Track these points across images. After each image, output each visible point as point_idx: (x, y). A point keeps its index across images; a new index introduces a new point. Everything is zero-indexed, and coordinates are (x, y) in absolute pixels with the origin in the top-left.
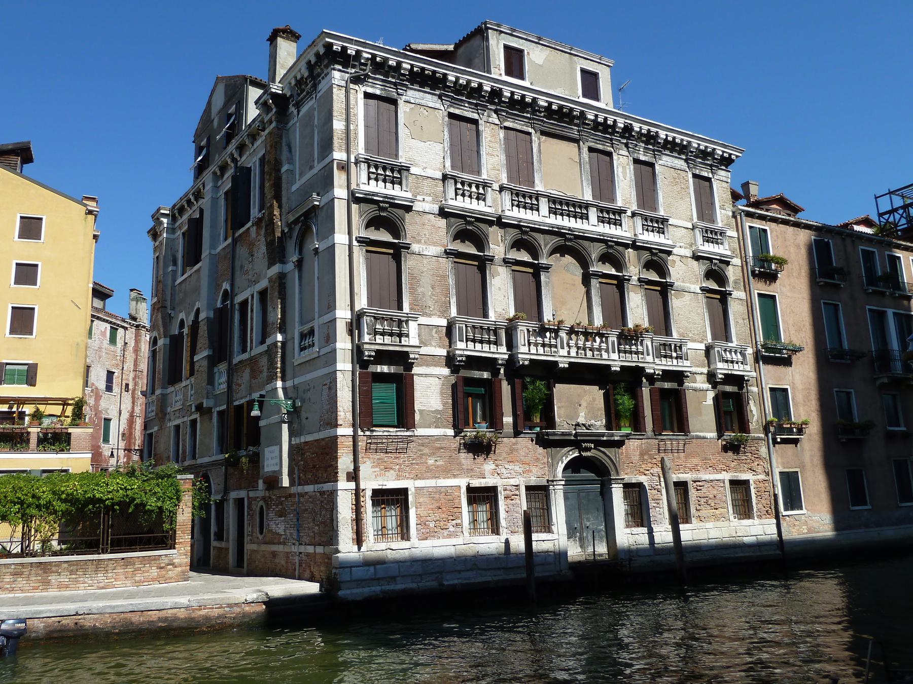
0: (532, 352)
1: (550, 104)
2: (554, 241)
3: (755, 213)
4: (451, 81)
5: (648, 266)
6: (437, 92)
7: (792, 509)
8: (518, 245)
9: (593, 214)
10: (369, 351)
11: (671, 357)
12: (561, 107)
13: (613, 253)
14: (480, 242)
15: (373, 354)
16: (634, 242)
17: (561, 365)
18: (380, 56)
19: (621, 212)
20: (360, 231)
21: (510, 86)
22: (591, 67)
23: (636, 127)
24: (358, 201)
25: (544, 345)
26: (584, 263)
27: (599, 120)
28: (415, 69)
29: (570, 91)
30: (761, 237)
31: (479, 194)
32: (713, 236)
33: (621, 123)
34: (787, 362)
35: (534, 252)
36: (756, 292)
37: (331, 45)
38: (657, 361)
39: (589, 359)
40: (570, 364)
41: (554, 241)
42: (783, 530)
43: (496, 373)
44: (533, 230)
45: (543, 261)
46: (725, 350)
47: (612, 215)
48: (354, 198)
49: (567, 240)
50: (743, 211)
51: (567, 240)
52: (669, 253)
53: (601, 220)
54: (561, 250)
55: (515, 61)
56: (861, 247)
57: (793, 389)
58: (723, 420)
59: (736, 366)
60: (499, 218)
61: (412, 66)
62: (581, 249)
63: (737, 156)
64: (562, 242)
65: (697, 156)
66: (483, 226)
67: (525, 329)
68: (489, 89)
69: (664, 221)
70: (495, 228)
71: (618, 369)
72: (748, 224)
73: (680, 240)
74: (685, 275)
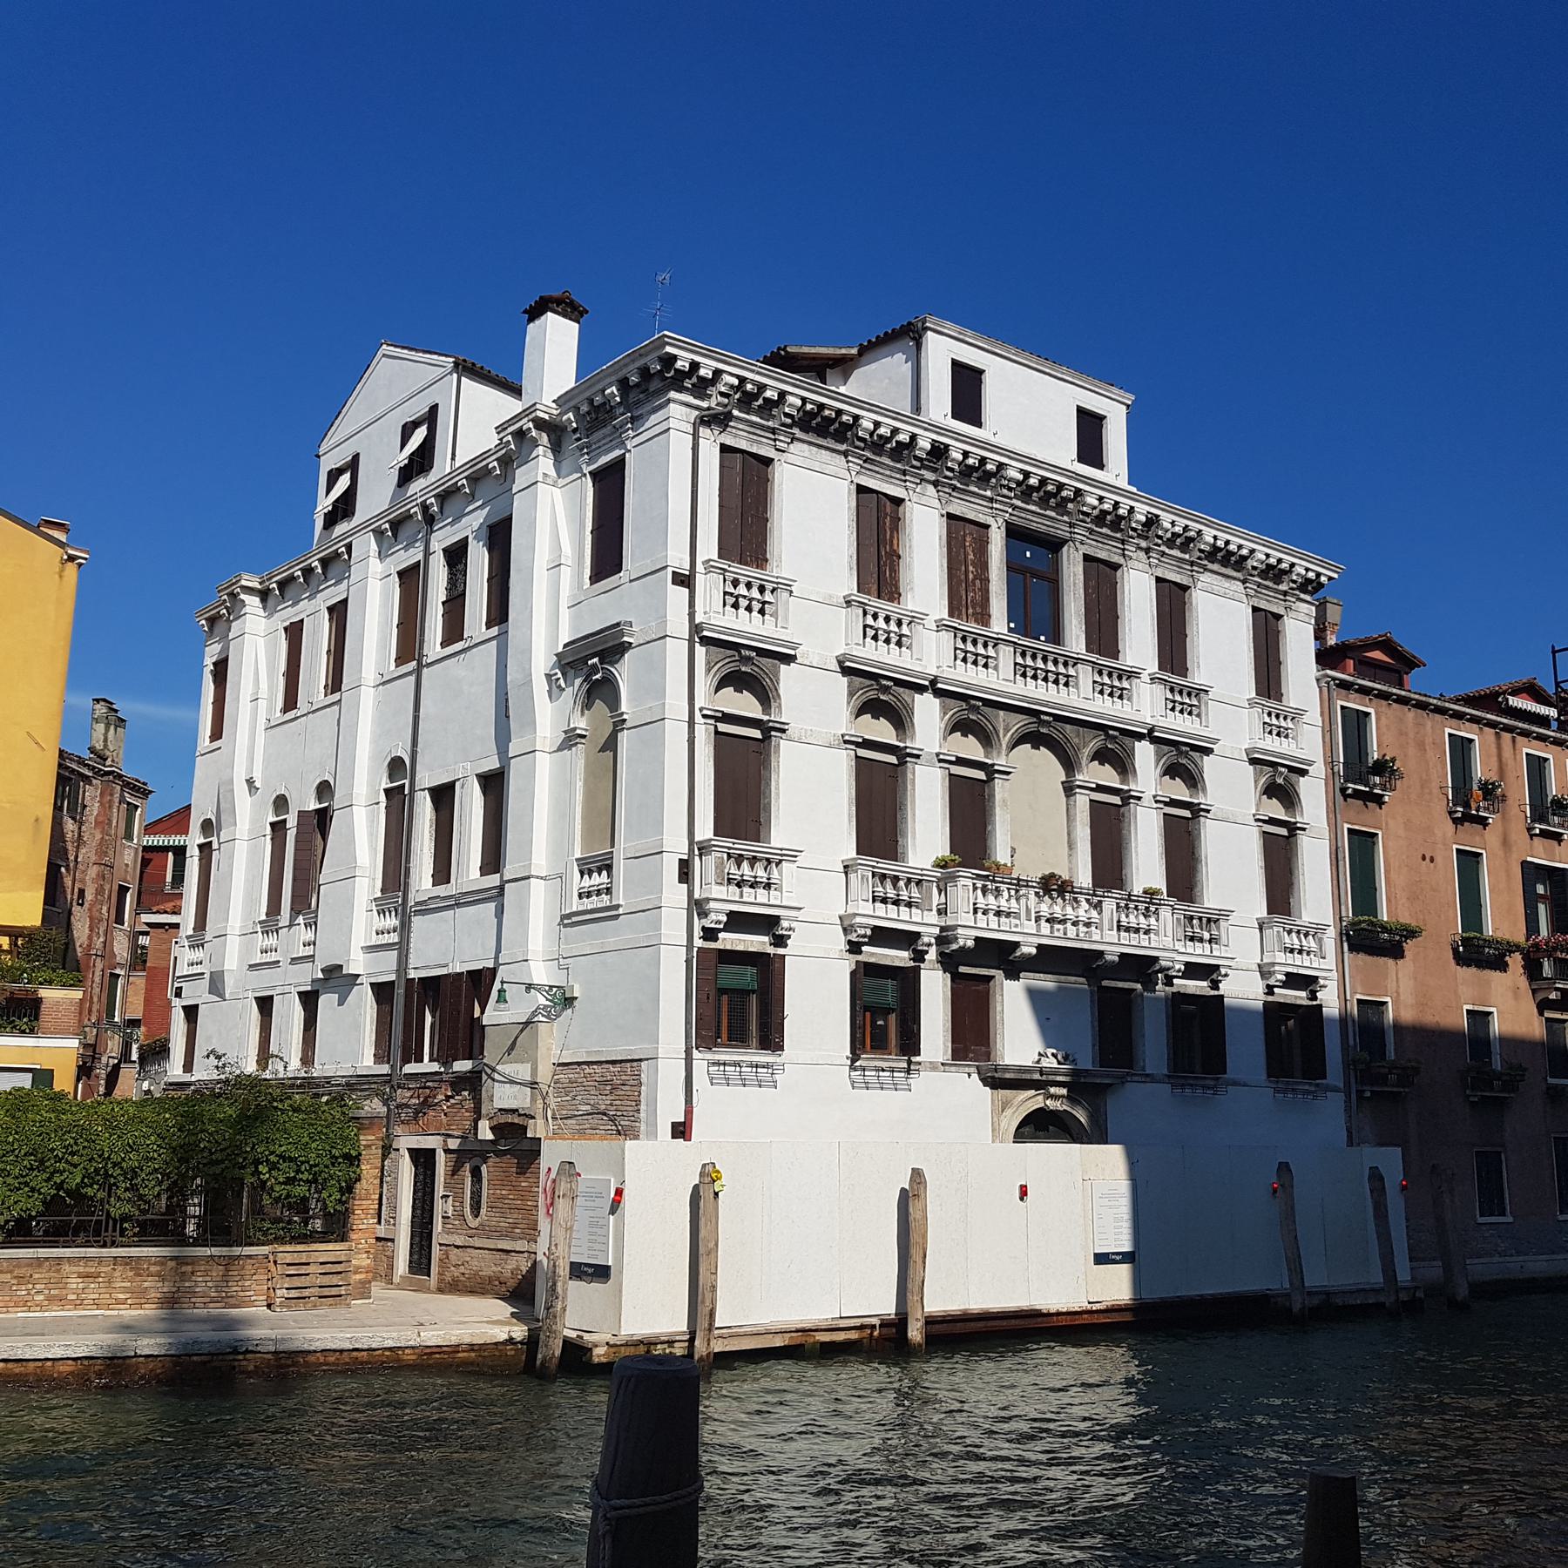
0: (1069, 935)
1: (1027, 475)
2: (1017, 723)
3: (1353, 684)
4: (865, 430)
5: (1172, 771)
6: (843, 447)
7: (1491, 1215)
8: (960, 726)
9: (1006, 656)
10: (965, 939)
11: (1201, 940)
12: (1044, 481)
13: (1115, 746)
14: (900, 719)
15: (869, 932)
16: (1151, 730)
17: (1109, 958)
18: (753, 382)
19: (1132, 675)
20: (703, 696)
21: (962, 439)
22: (1095, 403)
23: (1166, 519)
24: (706, 641)
25: (998, 914)
26: (1069, 765)
27: (1121, 511)
28: (809, 407)
29: (1058, 449)
30: (1356, 725)
31: (901, 636)
32: (1280, 722)
33: (1142, 511)
34: (1396, 952)
35: (987, 739)
36: (1346, 826)
37: (675, 358)
38: (1179, 946)
39: (1069, 937)
40: (1040, 947)
41: (1017, 723)
42: (702, 1270)
43: (919, 956)
44: (1057, 718)
45: (1000, 761)
46: (1290, 932)
47: (1118, 681)
48: (698, 634)
49: (1042, 723)
50: (1334, 679)
51: (1042, 723)
52: (1207, 751)
53: (1022, 671)
54: (1034, 739)
55: (967, 390)
56: (1525, 750)
57: (1395, 1003)
58: (859, 1020)
59: (1306, 961)
60: (934, 682)
61: (804, 400)
62: (1191, 767)
63: (1330, 579)
64: (1033, 727)
65: (1170, 543)
66: (905, 693)
67: (969, 883)
68: (1143, 519)
69: (1199, 692)
70: (928, 696)
71: (1034, 951)
72: (1340, 703)
73: (1231, 725)
74: (1231, 792)
